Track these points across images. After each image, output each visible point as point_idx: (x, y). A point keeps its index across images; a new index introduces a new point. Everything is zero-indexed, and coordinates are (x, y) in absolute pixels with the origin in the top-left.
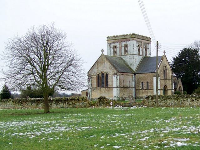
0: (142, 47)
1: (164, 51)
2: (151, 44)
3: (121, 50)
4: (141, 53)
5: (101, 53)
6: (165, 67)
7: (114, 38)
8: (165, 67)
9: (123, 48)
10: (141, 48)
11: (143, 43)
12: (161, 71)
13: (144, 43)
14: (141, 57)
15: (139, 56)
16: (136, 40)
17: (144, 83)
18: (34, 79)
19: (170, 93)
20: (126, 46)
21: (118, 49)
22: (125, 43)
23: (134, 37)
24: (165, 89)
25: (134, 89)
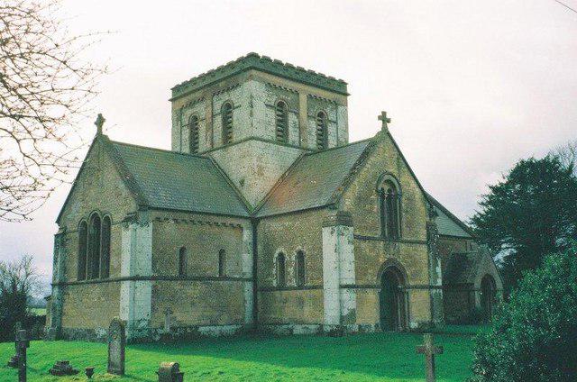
0: (297, 114)
1: (384, 113)
2: (346, 104)
3: (210, 127)
4: (293, 136)
5: (92, 132)
6: (388, 182)
7: (190, 88)
8: (388, 182)
9: (219, 120)
10: (292, 118)
11: (303, 98)
12: (360, 200)
13: (310, 97)
14: (294, 154)
15: (283, 148)
16: (261, 80)
17: (287, 258)
18: (227, 272)
19: (419, 308)
20: (228, 108)
21: (202, 127)
22: (225, 97)
23: (253, 65)
24: (392, 284)
25: (248, 286)
